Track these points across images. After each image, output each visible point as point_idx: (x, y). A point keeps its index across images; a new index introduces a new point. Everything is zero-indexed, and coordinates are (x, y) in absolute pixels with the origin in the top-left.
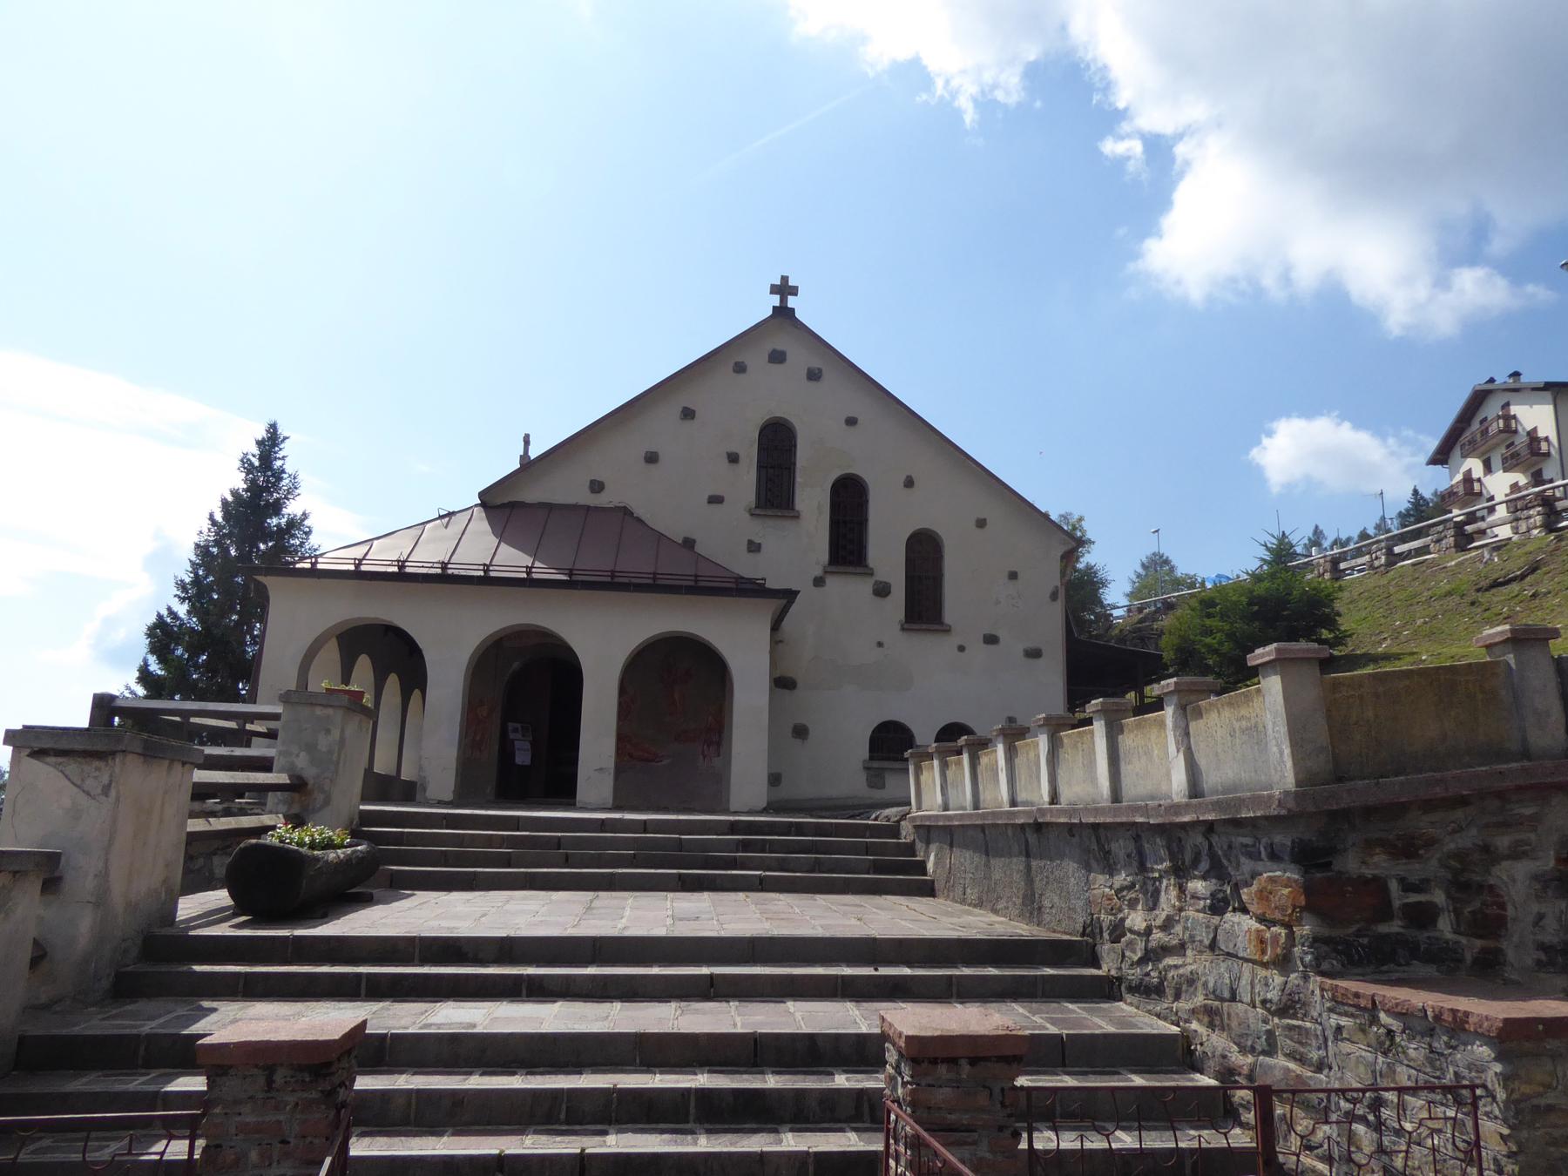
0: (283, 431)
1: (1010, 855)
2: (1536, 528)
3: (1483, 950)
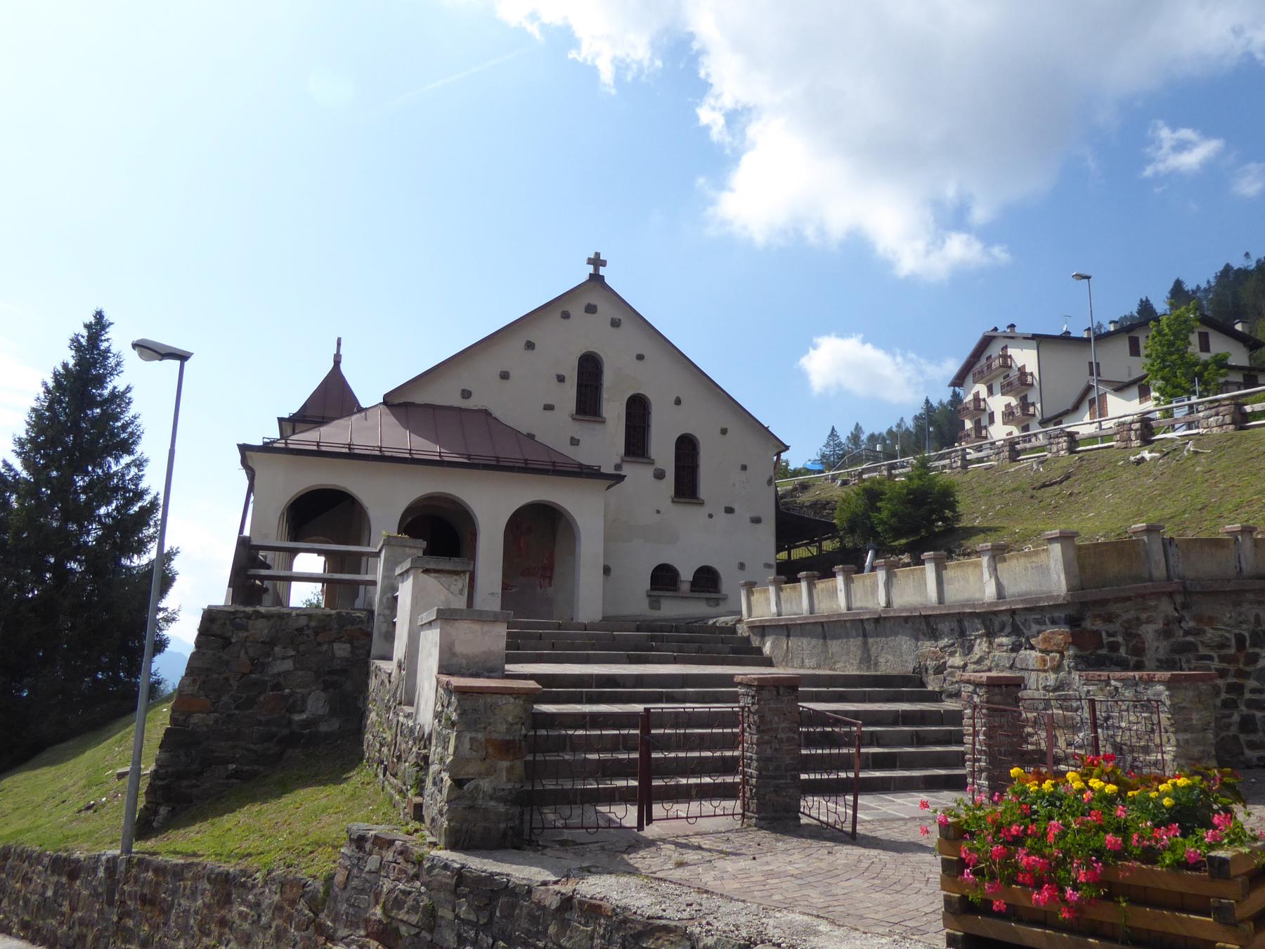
0: (108, 317)
1: (848, 636)
2: (1063, 450)
3: (1137, 662)
